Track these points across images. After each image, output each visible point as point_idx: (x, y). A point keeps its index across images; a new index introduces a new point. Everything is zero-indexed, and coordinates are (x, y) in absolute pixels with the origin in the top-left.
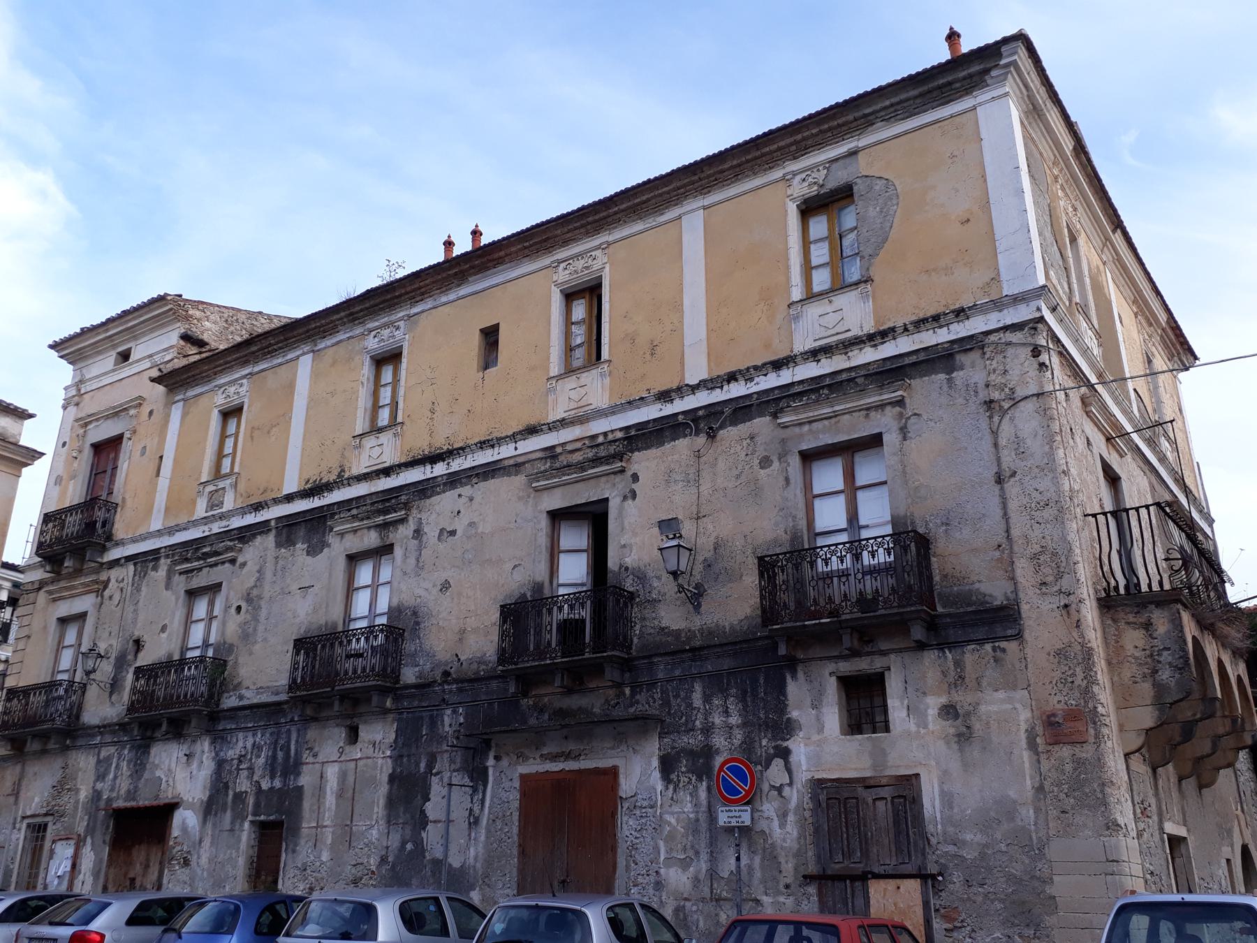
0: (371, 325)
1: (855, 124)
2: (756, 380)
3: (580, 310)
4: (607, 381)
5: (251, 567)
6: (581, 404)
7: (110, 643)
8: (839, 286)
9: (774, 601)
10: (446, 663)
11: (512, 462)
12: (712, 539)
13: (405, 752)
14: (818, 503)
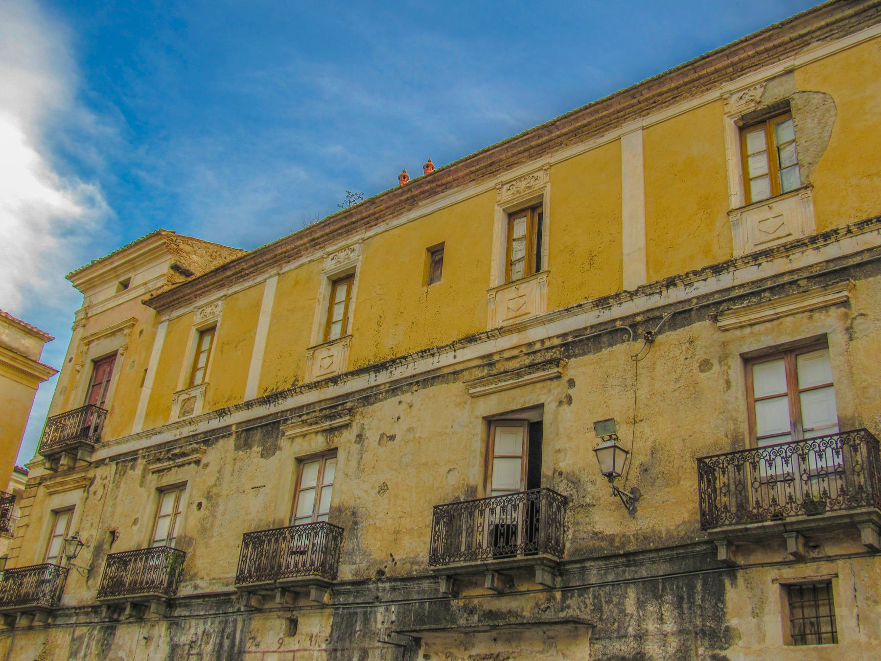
0: (330, 249)
1: (791, 45)
2: (696, 285)
3: (521, 227)
4: (545, 290)
5: (213, 467)
6: (519, 313)
7: (91, 533)
8: (778, 193)
9: (712, 506)
10: (381, 562)
11: (451, 370)
12: (649, 444)
13: (339, 647)
14: (759, 407)
